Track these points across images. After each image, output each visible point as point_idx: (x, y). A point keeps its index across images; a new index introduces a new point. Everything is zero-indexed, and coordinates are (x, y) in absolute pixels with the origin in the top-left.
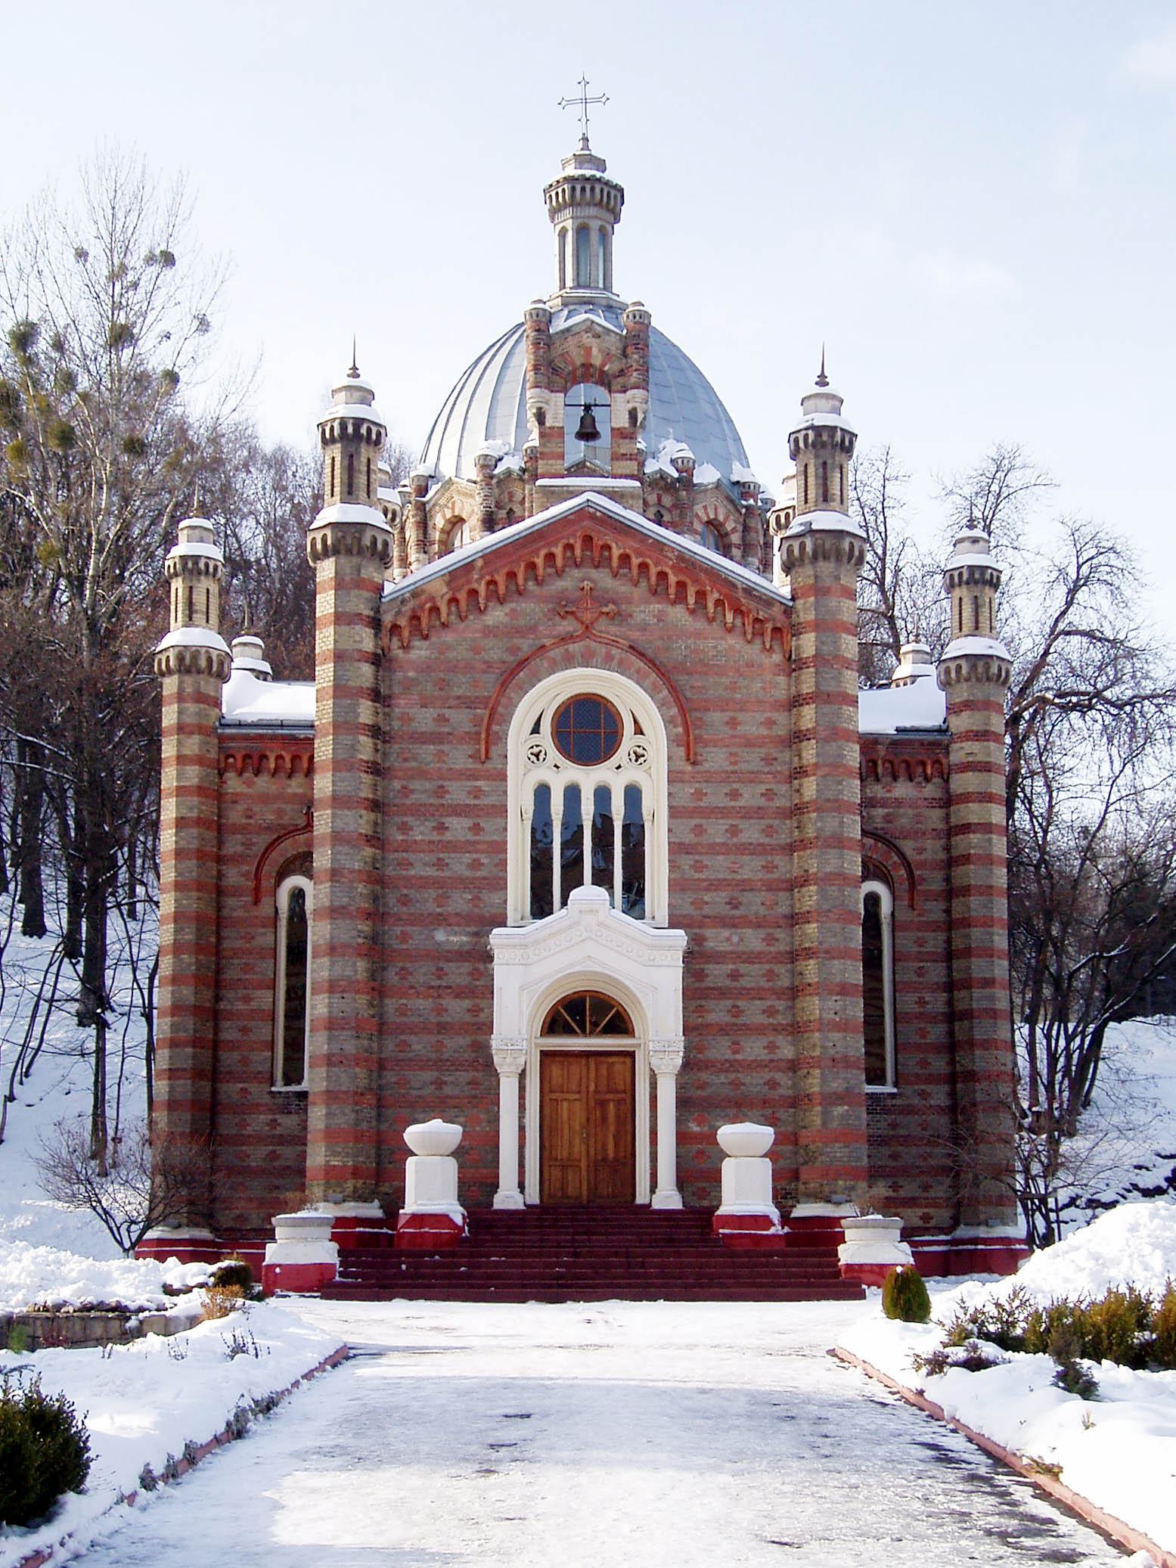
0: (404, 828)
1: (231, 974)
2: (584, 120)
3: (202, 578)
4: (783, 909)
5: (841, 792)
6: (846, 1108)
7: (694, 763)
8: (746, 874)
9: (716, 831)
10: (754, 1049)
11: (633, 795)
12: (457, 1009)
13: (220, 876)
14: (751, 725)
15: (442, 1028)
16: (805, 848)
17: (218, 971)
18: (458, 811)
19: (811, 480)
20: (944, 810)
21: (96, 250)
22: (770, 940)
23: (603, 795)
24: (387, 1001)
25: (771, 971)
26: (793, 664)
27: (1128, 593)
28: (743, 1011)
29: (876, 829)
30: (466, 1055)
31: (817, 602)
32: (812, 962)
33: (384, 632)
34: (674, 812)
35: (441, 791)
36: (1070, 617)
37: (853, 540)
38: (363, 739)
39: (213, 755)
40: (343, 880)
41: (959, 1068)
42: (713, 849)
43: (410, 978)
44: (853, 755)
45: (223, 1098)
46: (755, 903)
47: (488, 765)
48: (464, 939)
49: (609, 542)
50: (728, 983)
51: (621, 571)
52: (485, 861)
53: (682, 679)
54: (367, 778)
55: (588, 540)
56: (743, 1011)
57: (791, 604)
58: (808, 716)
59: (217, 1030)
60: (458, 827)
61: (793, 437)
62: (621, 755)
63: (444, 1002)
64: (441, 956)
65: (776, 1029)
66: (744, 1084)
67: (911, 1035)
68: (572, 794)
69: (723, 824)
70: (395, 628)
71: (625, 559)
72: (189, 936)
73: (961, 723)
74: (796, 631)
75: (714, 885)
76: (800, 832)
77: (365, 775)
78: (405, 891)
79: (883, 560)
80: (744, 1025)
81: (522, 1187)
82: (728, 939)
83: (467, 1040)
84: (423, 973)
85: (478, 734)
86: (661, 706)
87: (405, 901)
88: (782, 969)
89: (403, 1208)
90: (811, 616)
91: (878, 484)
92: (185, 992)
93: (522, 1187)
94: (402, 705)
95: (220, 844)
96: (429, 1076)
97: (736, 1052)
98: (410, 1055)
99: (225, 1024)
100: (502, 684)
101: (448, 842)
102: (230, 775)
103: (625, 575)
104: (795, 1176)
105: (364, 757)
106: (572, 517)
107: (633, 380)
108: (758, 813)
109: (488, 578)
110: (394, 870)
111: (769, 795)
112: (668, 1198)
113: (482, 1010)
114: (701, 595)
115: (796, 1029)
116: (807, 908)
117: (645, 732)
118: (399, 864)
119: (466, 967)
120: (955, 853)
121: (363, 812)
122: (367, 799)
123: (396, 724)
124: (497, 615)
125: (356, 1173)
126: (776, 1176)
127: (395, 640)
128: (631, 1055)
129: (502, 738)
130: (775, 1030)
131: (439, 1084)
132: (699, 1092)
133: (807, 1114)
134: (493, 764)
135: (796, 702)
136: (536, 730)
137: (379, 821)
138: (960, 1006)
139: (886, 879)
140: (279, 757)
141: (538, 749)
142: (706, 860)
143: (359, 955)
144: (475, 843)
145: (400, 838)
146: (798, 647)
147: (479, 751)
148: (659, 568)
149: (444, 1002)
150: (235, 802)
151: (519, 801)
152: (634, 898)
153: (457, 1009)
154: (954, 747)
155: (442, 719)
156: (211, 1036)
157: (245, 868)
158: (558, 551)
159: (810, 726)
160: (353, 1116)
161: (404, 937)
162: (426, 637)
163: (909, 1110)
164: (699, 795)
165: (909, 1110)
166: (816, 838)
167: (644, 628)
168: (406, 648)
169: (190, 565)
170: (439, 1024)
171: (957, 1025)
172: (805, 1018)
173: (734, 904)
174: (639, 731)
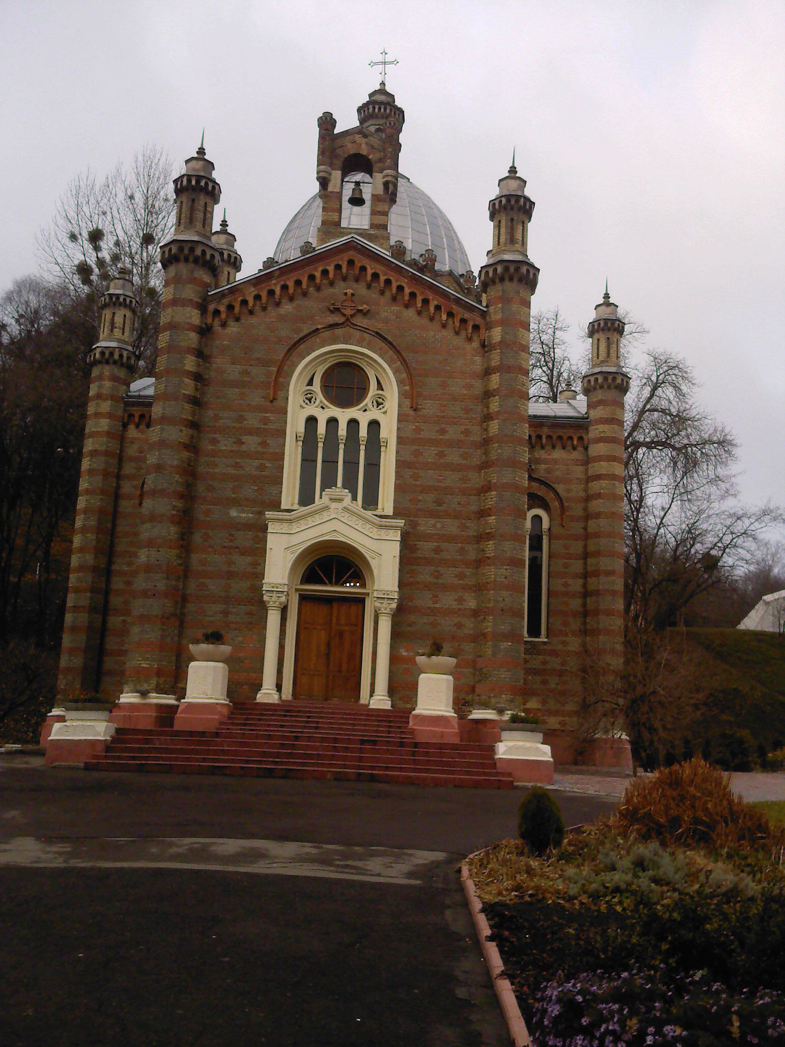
0: (214, 441)
1: (120, 547)
2: (383, 74)
4: (474, 508)
5: (515, 430)
6: (510, 644)
7: (415, 410)
9: (430, 454)
10: (448, 600)
11: (374, 425)
12: (242, 563)
13: (118, 487)
15: (231, 575)
16: (489, 467)
17: (112, 545)
18: (251, 432)
19: (503, 230)
20: (584, 467)
21: (139, 199)
22: (463, 527)
23: (353, 424)
25: (462, 548)
26: (485, 347)
27: (684, 388)
28: (441, 575)
29: (541, 477)
30: (246, 594)
31: (503, 308)
32: (491, 542)
33: (209, 314)
34: (400, 441)
35: (241, 419)
36: (655, 400)
37: (529, 268)
38: (187, 380)
39: (120, 413)
40: (165, 472)
41: (588, 627)
44: (525, 431)
45: (109, 625)
48: (251, 515)
49: (365, 265)
50: (433, 555)
51: (373, 284)
54: (188, 406)
55: (351, 263)
56: (441, 575)
57: (485, 309)
58: (495, 380)
59: (108, 581)
60: (251, 442)
61: (492, 203)
62: (368, 401)
64: (234, 526)
65: (466, 588)
66: (440, 624)
67: (558, 585)
69: (434, 450)
70: (217, 313)
71: (375, 276)
73: (595, 414)
74: (489, 327)
76: (486, 456)
77: (187, 404)
78: (211, 483)
79: (552, 371)
80: (442, 584)
81: (279, 687)
82: (434, 526)
85: (269, 383)
86: (396, 372)
87: (210, 489)
89: (184, 699)
90: (499, 316)
91: (550, 331)
92: (87, 557)
93: (279, 687)
94: (219, 362)
95: (120, 467)
96: (219, 607)
99: (115, 579)
100: (289, 350)
101: (244, 452)
102: (132, 427)
103: (375, 287)
104: (473, 689)
106: (342, 247)
107: (387, 164)
108: (458, 444)
110: (204, 468)
111: (467, 432)
112: (380, 701)
114: (426, 302)
115: (479, 588)
117: (384, 389)
118: (208, 465)
119: (250, 534)
120: (591, 492)
121: (183, 428)
122: (187, 420)
123: (213, 374)
124: (287, 308)
125: (159, 673)
126: (456, 689)
127: (217, 320)
128: (360, 601)
129: (286, 388)
130: (463, 588)
131: (226, 613)
132: (409, 628)
133: (482, 647)
134: (279, 403)
135: (488, 372)
136: (310, 383)
137: (195, 435)
138: (591, 588)
139: (546, 506)
142: (421, 473)
143: (172, 522)
144: (263, 453)
145: (210, 447)
146: (489, 337)
148: (399, 283)
150: (132, 443)
152: (371, 500)
153: (242, 563)
154: (591, 428)
156: (104, 586)
157: (135, 483)
158: (331, 269)
159: (496, 387)
160: (160, 633)
161: (207, 513)
162: (238, 319)
163: (553, 653)
164: (418, 430)
165: (553, 653)
166: (497, 460)
167: (386, 321)
168: (224, 325)
169: (114, 299)
170: (228, 572)
171: (588, 600)
173: (439, 502)
174: (380, 387)
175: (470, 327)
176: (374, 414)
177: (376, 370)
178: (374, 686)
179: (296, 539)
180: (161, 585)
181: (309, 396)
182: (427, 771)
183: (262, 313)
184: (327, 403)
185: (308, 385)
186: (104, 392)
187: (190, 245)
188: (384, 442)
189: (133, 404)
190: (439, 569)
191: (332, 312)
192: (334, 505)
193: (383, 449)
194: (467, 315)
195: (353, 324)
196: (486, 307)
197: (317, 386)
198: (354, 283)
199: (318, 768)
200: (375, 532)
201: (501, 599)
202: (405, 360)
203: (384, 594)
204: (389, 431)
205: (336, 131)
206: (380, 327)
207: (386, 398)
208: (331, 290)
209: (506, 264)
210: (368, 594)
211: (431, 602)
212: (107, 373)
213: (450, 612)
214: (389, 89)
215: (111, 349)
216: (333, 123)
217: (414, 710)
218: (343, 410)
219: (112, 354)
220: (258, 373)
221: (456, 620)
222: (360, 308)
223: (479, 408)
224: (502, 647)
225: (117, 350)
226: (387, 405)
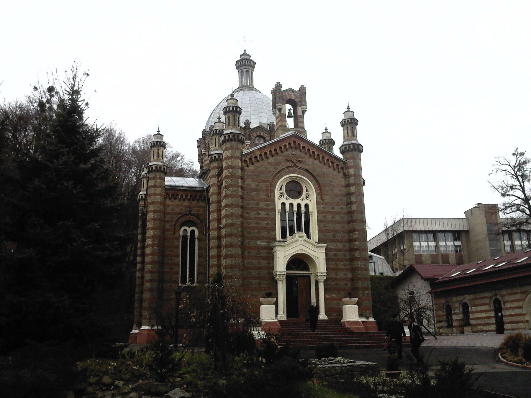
3: (162, 147)
7: (322, 200)
8: (337, 229)
9: (329, 217)
11: (307, 206)
13: (164, 226)
14: (336, 191)
15: (260, 268)
18: (262, 209)
19: (349, 131)
22: (344, 246)
23: (299, 206)
24: (245, 261)
32: (358, 252)
34: (318, 212)
35: (258, 204)
39: (164, 194)
42: (329, 222)
43: (251, 254)
46: (339, 236)
47: (270, 198)
48: (265, 243)
49: (300, 143)
52: (270, 223)
53: (318, 179)
55: (294, 142)
57: (345, 161)
60: (263, 214)
62: (303, 196)
63: (260, 261)
64: (258, 248)
65: (347, 270)
68: (291, 205)
72: (156, 242)
74: (347, 168)
75: (329, 231)
82: (333, 245)
83: (266, 272)
84: (254, 253)
87: (249, 233)
88: (347, 254)
94: (248, 181)
95: (165, 217)
97: (337, 276)
98: (252, 276)
105: (240, 194)
108: (339, 213)
109: (270, 150)
111: (341, 208)
113: (271, 263)
116: (355, 238)
124: (271, 160)
128: (308, 277)
139: (195, 225)
140: (182, 195)
141: (282, 194)
146: (348, 172)
147: (268, 194)
148: (313, 150)
149: (260, 261)
150: (168, 206)
151: (278, 207)
155: (258, 185)
161: (249, 243)
162: (253, 164)
164: (324, 208)
167: (308, 165)
172: (355, 267)
173: (334, 236)
175: (340, 168)
176: (306, 201)
177: (306, 184)
178: (278, 308)
179: (287, 253)
180: (238, 273)
181: (281, 194)
182: (373, 343)
183: (262, 162)
184: (288, 197)
185: (280, 190)
186: (158, 184)
187: (237, 134)
188: (311, 212)
189: (169, 189)
190: (337, 262)
191: (288, 161)
192: (300, 239)
193: (310, 215)
194: (338, 163)
195: (297, 166)
196: (346, 160)
197: (284, 190)
198: (295, 150)
199: (376, 345)
200: (316, 249)
201: (363, 274)
202: (317, 181)
203: (322, 274)
204: (313, 208)
205: (283, 89)
206: (307, 167)
207: (309, 195)
208: (287, 153)
209: (354, 145)
210: (312, 273)
211: (335, 276)
212: (158, 176)
213: (342, 280)
214: (248, 52)
215: (160, 166)
216: (281, 86)
217: (342, 320)
218: (295, 200)
219: (160, 168)
220: (263, 186)
221: (345, 282)
222: (299, 160)
223: (345, 199)
224: (366, 293)
225: (163, 166)
226: (310, 198)
